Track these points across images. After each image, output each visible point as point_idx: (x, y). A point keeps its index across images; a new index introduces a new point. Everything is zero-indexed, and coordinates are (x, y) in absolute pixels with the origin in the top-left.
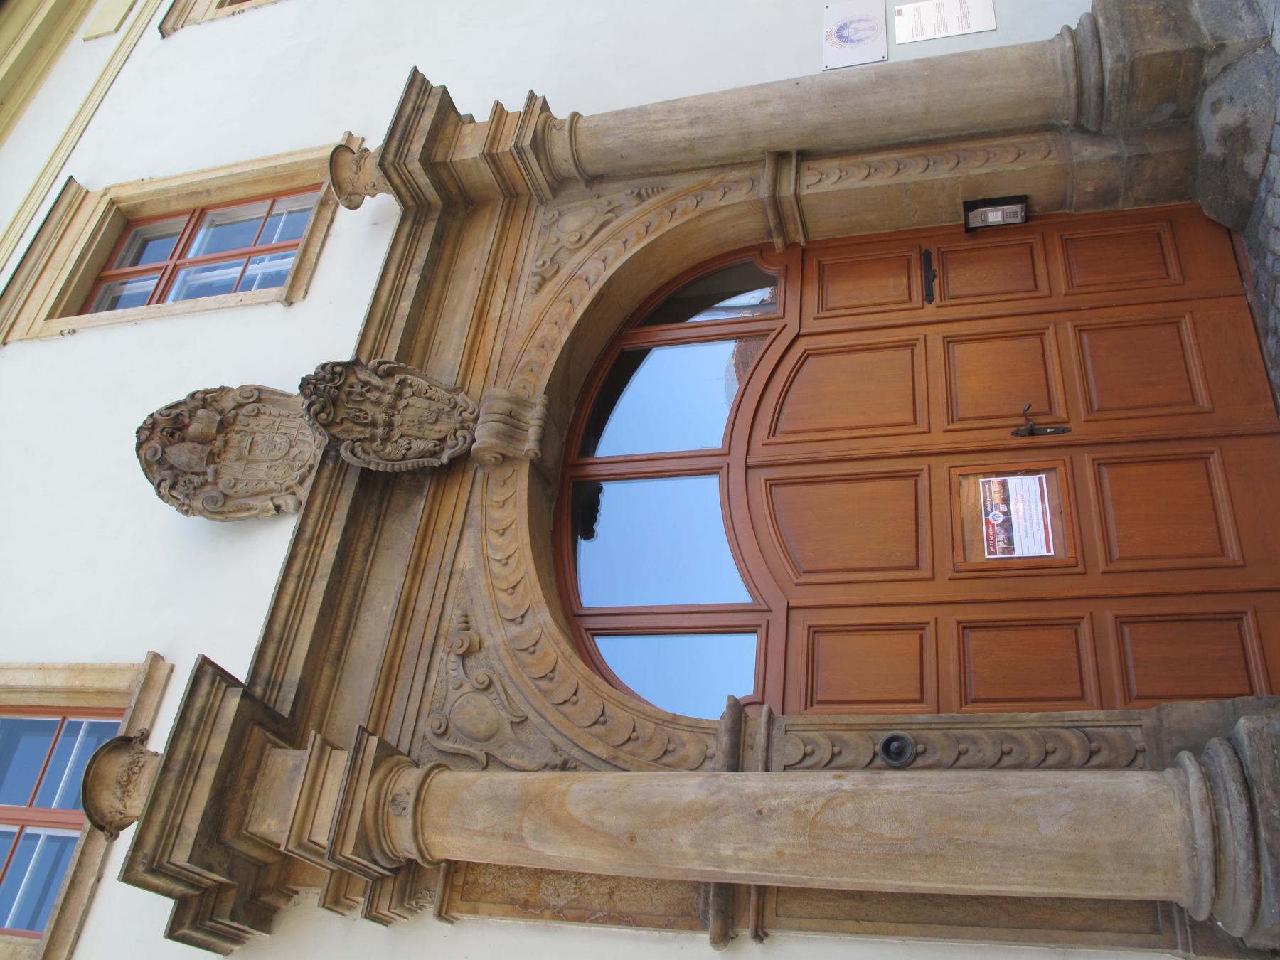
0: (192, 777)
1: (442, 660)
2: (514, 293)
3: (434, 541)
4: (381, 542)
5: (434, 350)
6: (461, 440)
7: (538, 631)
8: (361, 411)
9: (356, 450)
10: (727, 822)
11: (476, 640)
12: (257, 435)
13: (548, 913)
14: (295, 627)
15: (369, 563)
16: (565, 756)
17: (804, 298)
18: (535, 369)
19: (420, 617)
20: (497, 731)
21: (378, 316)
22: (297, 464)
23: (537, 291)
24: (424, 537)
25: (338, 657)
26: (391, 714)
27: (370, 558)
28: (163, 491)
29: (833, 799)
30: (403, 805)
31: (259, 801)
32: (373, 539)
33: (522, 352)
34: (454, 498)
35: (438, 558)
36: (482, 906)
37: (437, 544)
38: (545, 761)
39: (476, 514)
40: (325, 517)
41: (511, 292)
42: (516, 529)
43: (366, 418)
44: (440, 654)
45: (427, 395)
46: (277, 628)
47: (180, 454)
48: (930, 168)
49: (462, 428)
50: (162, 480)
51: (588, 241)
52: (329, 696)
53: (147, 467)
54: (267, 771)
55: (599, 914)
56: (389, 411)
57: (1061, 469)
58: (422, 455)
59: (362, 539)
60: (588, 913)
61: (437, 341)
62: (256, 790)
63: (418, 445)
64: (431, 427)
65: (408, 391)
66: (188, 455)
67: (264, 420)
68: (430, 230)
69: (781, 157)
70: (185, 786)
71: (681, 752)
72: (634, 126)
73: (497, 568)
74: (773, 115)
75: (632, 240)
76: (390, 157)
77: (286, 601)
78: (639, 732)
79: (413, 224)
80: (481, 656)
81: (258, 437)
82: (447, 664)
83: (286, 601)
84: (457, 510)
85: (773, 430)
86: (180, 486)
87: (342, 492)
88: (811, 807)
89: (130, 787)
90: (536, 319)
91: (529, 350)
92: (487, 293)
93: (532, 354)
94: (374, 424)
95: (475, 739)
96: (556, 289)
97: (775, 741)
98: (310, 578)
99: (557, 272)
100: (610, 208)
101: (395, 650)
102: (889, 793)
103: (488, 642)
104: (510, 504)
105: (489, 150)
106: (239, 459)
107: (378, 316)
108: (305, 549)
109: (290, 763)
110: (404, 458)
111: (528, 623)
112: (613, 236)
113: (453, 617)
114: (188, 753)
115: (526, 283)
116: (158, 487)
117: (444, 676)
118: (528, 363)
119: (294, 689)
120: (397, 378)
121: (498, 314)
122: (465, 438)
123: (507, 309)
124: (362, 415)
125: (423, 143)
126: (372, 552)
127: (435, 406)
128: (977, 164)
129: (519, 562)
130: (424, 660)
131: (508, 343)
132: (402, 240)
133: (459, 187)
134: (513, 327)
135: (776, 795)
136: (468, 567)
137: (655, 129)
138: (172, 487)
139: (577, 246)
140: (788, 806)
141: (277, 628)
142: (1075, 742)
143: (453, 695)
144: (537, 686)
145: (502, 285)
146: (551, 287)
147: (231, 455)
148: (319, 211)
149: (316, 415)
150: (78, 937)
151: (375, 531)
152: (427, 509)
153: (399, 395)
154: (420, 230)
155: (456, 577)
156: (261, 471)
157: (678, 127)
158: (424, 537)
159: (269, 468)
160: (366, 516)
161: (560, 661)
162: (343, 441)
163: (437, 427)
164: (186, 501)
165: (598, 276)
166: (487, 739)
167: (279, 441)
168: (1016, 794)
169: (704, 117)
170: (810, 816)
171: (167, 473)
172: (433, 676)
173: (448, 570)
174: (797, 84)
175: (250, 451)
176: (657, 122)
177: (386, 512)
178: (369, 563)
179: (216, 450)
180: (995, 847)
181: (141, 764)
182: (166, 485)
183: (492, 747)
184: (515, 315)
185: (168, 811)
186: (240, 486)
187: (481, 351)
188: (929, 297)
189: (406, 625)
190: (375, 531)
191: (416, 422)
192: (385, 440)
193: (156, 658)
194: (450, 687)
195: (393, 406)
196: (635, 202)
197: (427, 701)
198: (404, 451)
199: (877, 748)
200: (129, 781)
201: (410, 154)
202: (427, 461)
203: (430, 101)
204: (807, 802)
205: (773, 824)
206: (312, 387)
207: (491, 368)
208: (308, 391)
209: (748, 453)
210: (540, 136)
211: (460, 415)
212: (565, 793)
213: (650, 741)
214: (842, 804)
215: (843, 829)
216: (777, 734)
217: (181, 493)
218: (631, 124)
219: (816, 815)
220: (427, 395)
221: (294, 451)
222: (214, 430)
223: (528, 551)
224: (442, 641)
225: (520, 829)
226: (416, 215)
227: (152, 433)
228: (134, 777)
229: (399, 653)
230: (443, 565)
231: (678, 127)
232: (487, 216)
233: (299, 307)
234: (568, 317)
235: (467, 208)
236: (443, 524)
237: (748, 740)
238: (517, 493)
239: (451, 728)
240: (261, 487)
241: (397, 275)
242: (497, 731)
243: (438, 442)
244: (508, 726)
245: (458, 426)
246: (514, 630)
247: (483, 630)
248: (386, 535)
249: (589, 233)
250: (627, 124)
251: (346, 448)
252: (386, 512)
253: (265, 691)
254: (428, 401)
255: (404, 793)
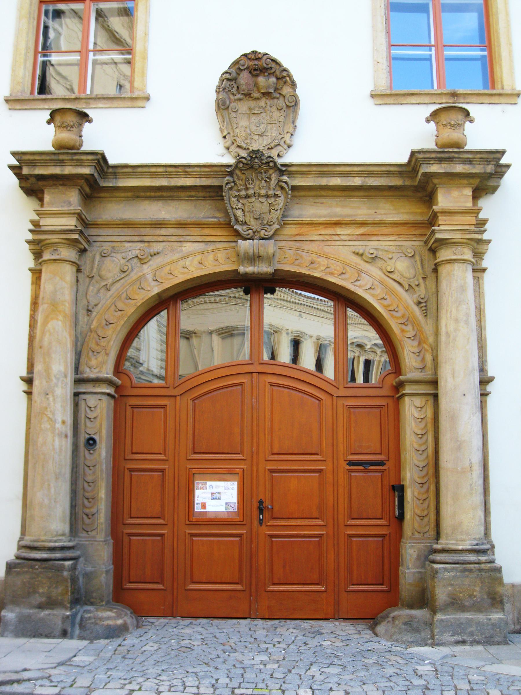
0: (55, 164)
1: (136, 246)
2: (354, 239)
3: (197, 229)
4: (199, 201)
5: (317, 201)
6: (247, 233)
7: (149, 289)
8: (253, 181)
9: (229, 184)
10: (44, 382)
11: (145, 261)
12: (265, 114)
13: (32, 313)
14: (143, 177)
15: (187, 198)
16: (93, 310)
17: (380, 398)
18: (297, 262)
19: (158, 232)
20: (103, 279)
21: (325, 169)
22: (248, 141)
23: (354, 252)
24: (199, 224)
25: (138, 197)
26: (111, 229)
27: (190, 198)
28: (224, 76)
29: (52, 420)
30: (54, 253)
31: (56, 190)
32: (199, 197)
33: (310, 252)
34: (220, 233)
35: (188, 233)
36: (34, 286)
37: (196, 231)
38: (90, 302)
39: (211, 247)
40: (200, 174)
41: (354, 238)
42: (202, 269)
43: (249, 183)
44: (139, 245)
45: (272, 210)
46: (140, 170)
47: (244, 78)
48: (418, 468)
49: (254, 232)
50: (230, 74)
51: (388, 277)
52: (120, 198)
53: (236, 63)
54: (68, 190)
55: (32, 333)
56: (257, 194)
57: (238, 519)
58: (235, 216)
59: (197, 193)
60: (32, 328)
61: (324, 201)
62: (60, 188)
63: (239, 214)
64: (252, 217)
65: (272, 200)
66: (244, 83)
67: (276, 114)
68: (397, 182)
69: (435, 383)
70: (51, 163)
71: (93, 358)
72: (450, 298)
73: (181, 263)
74: (446, 381)
75: (386, 303)
76: (421, 156)
77: (153, 170)
78: (103, 340)
79: (399, 172)
80: (139, 264)
81: (264, 115)
82: (135, 249)
83: (153, 170)
84: (214, 237)
85: (272, 385)
86: (229, 83)
87: (215, 179)
88: (49, 413)
89: (61, 128)
90: (331, 256)
91: (310, 256)
92: (354, 224)
93: (307, 258)
94: (247, 189)
95: (99, 270)
96: (352, 264)
97: (96, 396)
98: (168, 176)
99: (367, 262)
100: (413, 286)
101: (140, 224)
102: (54, 440)
103: (145, 266)
104: (216, 263)
105: (438, 212)
106: (250, 109)
107: (325, 169)
108: (180, 171)
109: (71, 200)
110: (232, 208)
111: (154, 283)
112: (391, 291)
113: (157, 247)
114: (63, 160)
115: (360, 246)
116: (226, 73)
117: (128, 250)
118: (301, 257)
119: (115, 185)
120: (278, 193)
121: (338, 233)
122: (249, 234)
123: (342, 237)
124: (251, 182)
125: (439, 171)
126: (193, 198)
127: (266, 217)
128: (416, 494)
129: (184, 273)
130: (136, 238)
131: (318, 243)
132: (384, 169)
133: (433, 190)
134: (329, 243)
135: (54, 400)
136: (184, 249)
137: (447, 311)
138: (228, 80)
139: (385, 271)
140: (49, 404)
141: (140, 170)
142: (92, 510)
143: (119, 256)
144: (123, 293)
145: (361, 231)
146: (357, 260)
147: (251, 103)
148: (445, 94)
149: (241, 162)
150: (26, 109)
151: (204, 197)
152: (212, 222)
153: (267, 196)
154: (395, 176)
155: (179, 244)
156: (244, 123)
157: (446, 325)
158: (199, 224)
159: (245, 127)
160: (210, 192)
161: (134, 301)
162: (233, 177)
163: (252, 220)
164: (221, 90)
165: (360, 287)
166: (99, 276)
167: (261, 127)
168: (52, 485)
169: (449, 341)
170: (46, 413)
171: (234, 74)
172: (130, 244)
173: (182, 240)
174: (464, 395)
175: (254, 114)
176: (451, 312)
177: (216, 200)
178: (187, 198)
179: (252, 95)
180: (34, 476)
181: (71, 129)
182: (227, 76)
183: (97, 278)
184: (338, 243)
185: (39, 160)
186: (233, 115)
187: (314, 228)
188: (351, 463)
189: (153, 226)
190: (204, 197)
191: (252, 209)
192: (239, 197)
193: (148, 99)
194: (123, 254)
195: (259, 196)
196: (415, 301)
197: (119, 244)
198: (234, 207)
199: (92, 436)
200: (66, 127)
201: (429, 165)
202: (233, 219)
203: (477, 166)
204: (51, 411)
205: (43, 399)
206: (254, 156)
207: (302, 236)
208: (251, 155)
209: (259, 373)
210: (447, 241)
211: (262, 229)
212: (57, 319)
213: (98, 345)
214: (50, 424)
215: (41, 424)
216: (99, 397)
217: (225, 85)
218: (452, 298)
219: (46, 415)
220: (272, 210)
221: (256, 137)
222: (262, 91)
223: (189, 277)
224: (146, 244)
225: (45, 303)
226: (406, 172)
227: (253, 59)
228: (65, 129)
229: (139, 226)
230: (184, 237)
231: (446, 325)
232: (419, 211)
233: (371, 101)
234: (332, 274)
235: (426, 196)
236: (207, 231)
237: (97, 385)
238: (222, 266)
239: (104, 258)
240: (235, 126)
241: (358, 172)
242: (103, 279)
243: (244, 222)
244: (105, 283)
245: (254, 230)
246: (150, 277)
247: (151, 263)
248: (203, 203)
249: (394, 276)
250: (452, 294)
251: (228, 180)
252: (216, 200)
253: (111, 173)
254: (267, 211)
255: (59, 252)
